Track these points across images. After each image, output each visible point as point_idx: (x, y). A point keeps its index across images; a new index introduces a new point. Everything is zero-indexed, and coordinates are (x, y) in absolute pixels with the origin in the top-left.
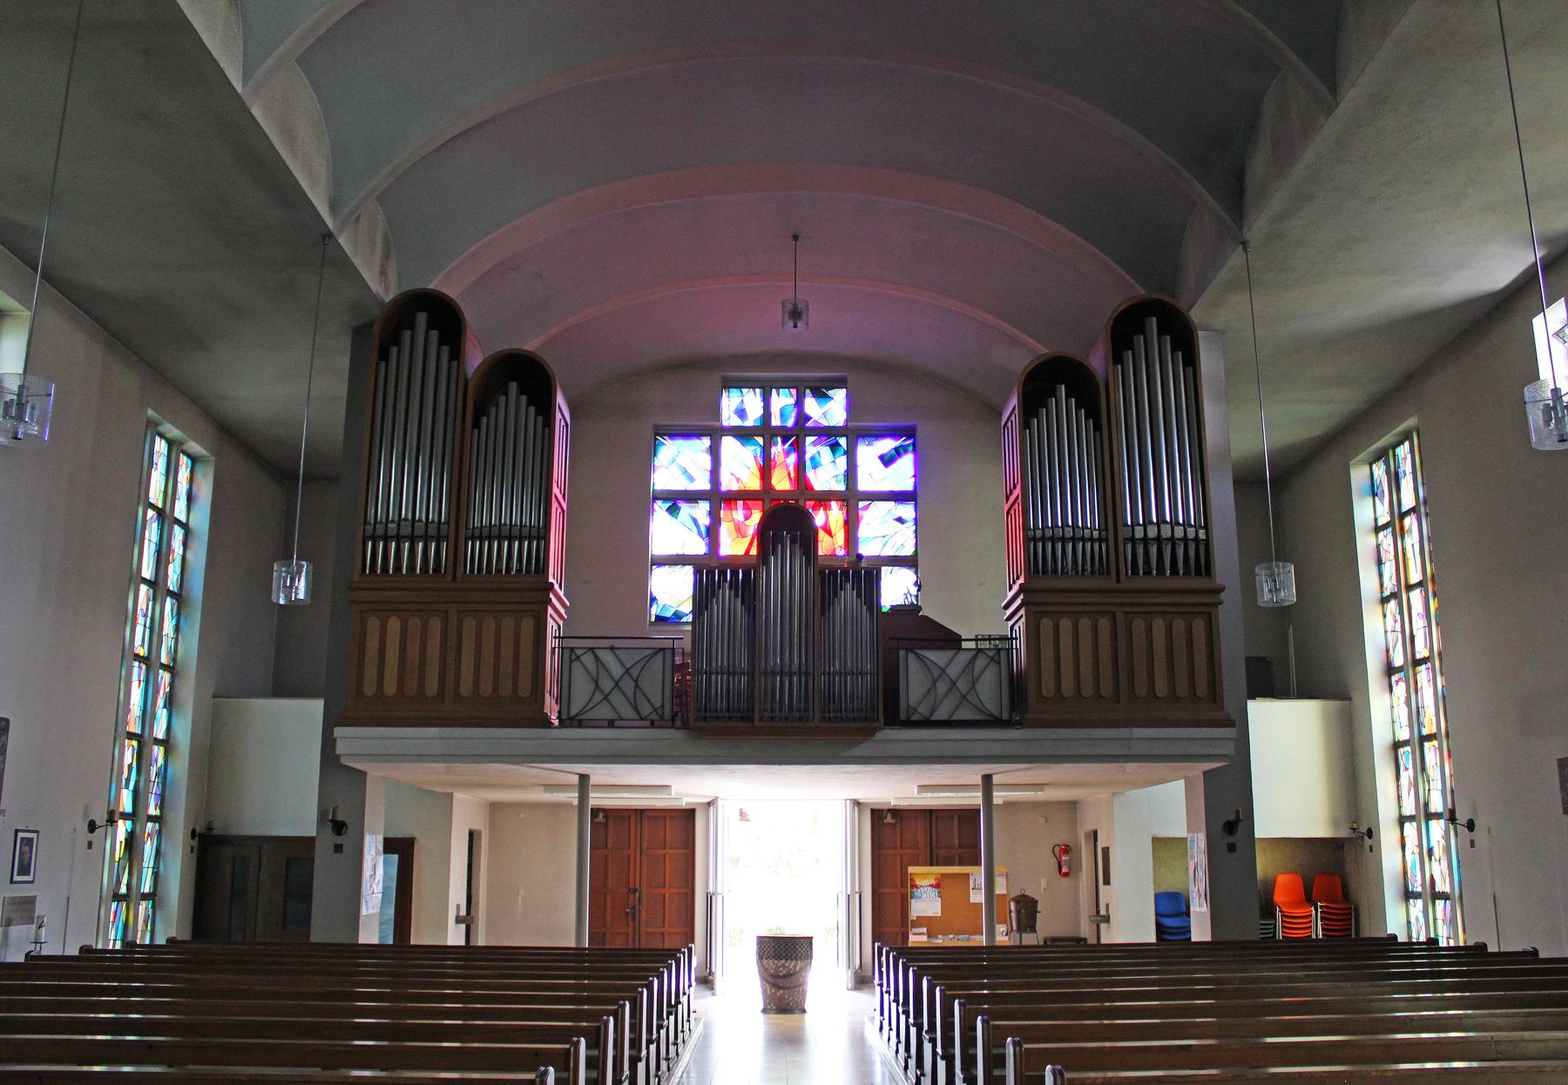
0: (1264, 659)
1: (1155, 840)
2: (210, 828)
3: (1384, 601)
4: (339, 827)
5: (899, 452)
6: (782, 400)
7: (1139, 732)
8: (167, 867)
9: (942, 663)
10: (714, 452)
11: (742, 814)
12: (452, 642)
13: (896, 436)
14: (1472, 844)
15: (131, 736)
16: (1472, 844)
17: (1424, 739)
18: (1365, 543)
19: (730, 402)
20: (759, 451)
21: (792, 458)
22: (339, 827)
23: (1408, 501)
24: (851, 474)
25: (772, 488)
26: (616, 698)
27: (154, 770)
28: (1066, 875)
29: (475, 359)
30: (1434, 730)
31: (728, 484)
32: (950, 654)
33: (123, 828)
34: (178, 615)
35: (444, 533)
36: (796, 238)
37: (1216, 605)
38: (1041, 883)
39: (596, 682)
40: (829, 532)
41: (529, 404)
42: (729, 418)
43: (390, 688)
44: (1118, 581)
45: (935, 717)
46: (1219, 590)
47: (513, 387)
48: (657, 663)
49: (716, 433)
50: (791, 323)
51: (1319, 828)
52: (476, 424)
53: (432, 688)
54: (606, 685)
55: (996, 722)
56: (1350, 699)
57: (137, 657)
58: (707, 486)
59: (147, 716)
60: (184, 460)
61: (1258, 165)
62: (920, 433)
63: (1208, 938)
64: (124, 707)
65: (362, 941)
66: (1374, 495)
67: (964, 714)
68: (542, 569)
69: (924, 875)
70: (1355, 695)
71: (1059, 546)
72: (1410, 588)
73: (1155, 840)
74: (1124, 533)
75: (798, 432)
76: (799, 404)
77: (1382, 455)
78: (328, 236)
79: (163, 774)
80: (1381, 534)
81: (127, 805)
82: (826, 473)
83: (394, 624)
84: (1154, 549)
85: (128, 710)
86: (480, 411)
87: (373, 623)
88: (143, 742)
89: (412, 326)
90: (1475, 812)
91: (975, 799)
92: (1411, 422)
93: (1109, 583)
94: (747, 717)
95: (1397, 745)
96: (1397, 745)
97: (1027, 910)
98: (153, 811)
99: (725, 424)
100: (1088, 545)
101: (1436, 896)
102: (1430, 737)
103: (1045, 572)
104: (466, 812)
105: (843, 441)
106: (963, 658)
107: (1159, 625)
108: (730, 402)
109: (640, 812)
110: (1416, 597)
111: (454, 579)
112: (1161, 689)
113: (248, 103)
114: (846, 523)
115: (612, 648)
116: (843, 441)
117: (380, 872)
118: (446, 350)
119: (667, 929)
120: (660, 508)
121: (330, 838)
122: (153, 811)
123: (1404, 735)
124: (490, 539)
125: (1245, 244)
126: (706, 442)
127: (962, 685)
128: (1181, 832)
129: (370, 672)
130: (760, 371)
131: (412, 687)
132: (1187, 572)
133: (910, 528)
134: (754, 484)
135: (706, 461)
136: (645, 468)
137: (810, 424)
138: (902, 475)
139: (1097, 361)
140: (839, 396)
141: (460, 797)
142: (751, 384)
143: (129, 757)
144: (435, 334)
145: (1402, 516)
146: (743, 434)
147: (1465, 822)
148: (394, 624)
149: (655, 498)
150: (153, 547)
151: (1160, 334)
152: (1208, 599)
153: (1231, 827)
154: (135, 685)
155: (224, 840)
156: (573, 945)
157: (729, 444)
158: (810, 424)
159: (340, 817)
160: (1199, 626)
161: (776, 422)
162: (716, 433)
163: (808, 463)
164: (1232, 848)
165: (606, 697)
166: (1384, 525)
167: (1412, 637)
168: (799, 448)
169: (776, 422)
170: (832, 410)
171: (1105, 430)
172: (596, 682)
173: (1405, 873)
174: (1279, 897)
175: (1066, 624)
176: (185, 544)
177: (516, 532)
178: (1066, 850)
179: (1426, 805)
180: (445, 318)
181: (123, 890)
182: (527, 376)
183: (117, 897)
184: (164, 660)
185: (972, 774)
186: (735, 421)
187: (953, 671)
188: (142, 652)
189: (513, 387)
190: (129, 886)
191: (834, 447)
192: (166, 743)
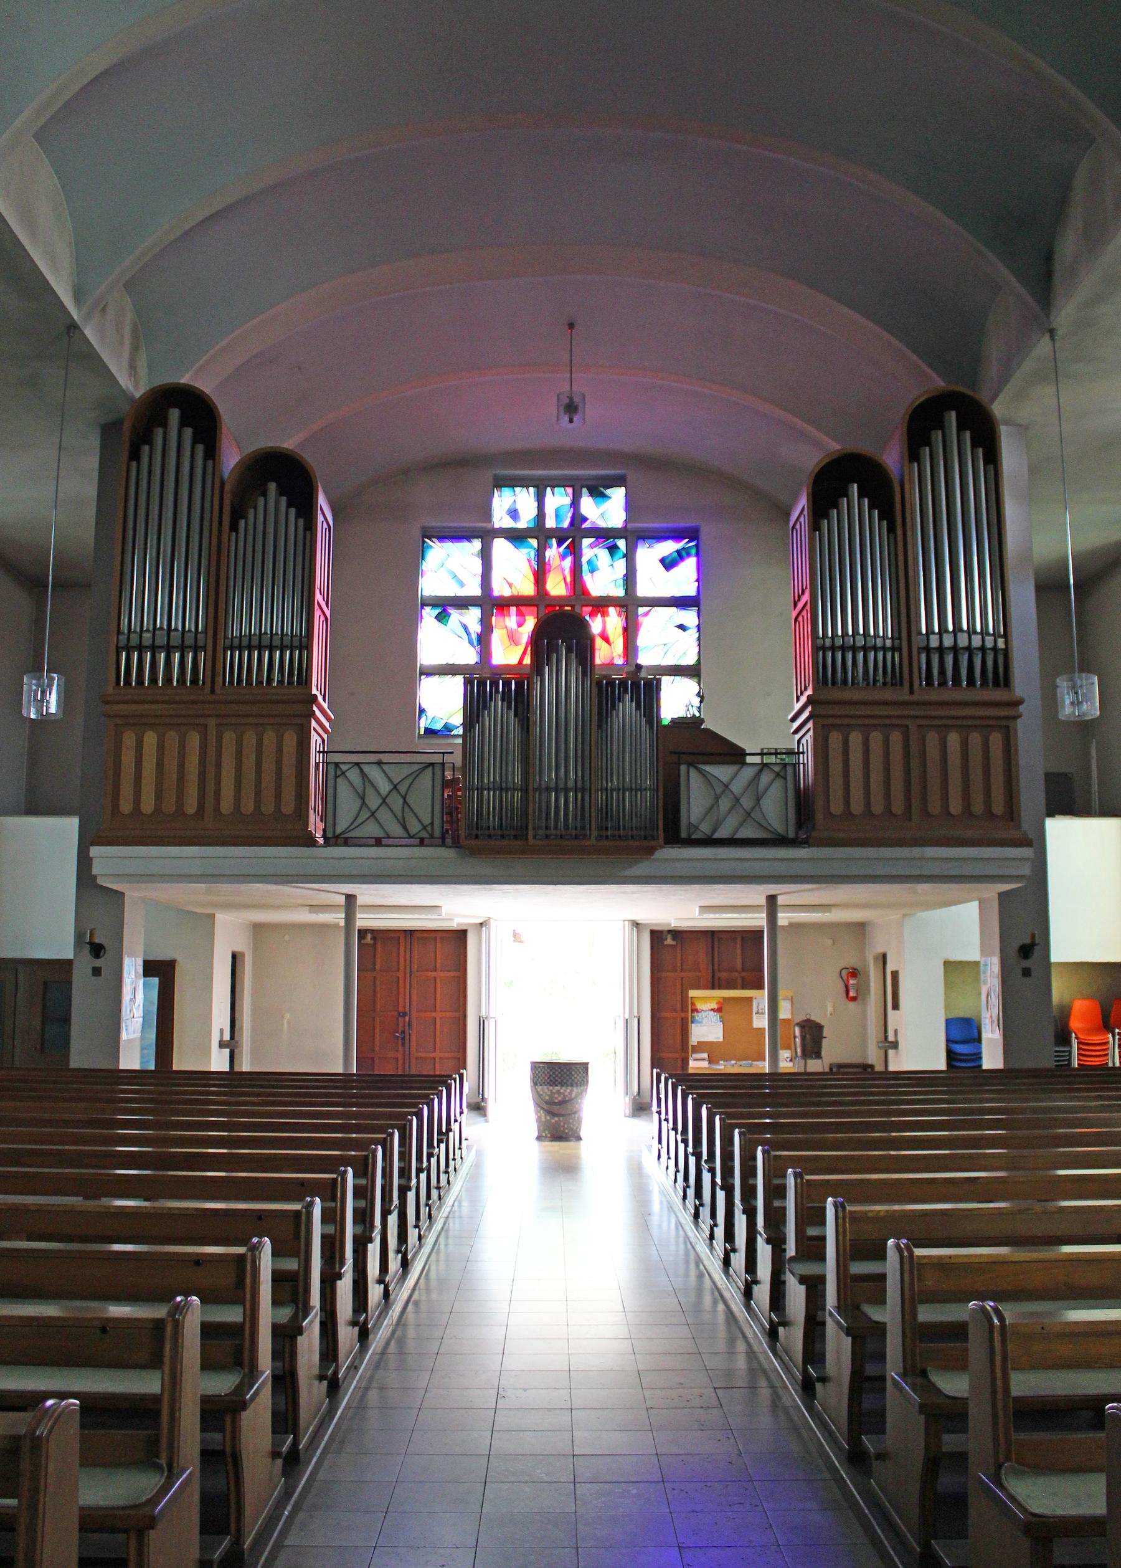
0: (1064, 775)
1: (947, 964)
4: (97, 950)
5: (681, 556)
6: (558, 500)
10: (486, 556)
13: (677, 538)
20: (533, 554)
21: (568, 562)
22: (97, 950)
24: (630, 579)
25: (547, 593)
26: (384, 815)
28: (854, 999)
29: (231, 459)
31: (500, 589)
35: (201, 643)
36: (571, 326)
38: (827, 1009)
39: (363, 798)
40: (606, 639)
42: (500, 519)
43: (148, 805)
44: (912, 692)
45: (717, 835)
47: (272, 487)
49: (487, 535)
50: (567, 418)
52: (234, 528)
53: (191, 807)
54: (373, 802)
55: (781, 841)
61: (1068, 247)
63: (1000, 1065)
68: (304, 680)
69: (705, 999)
73: (947, 964)
75: (574, 534)
76: (575, 504)
82: (604, 577)
83: (151, 739)
84: (949, 660)
86: (238, 514)
91: (759, 920)
93: (903, 695)
94: (520, 834)
97: (812, 1036)
100: (880, 655)
104: (229, 933)
105: (621, 543)
106: (747, 773)
107: (953, 738)
109: (410, 934)
111: (213, 691)
112: (956, 808)
114: (625, 630)
116: (621, 543)
118: (200, 448)
120: (429, 614)
125: (1052, 332)
126: (477, 544)
127: (746, 802)
130: (534, 468)
132: (984, 683)
134: (527, 588)
135: (477, 565)
136: (413, 573)
137: (586, 525)
138: (684, 579)
139: (892, 458)
140: (618, 495)
142: (524, 483)
146: (516, 537)
149: (423, 605)
153: (1026, 951)
157: (501, 547)
158: (586, 525)
159: (97, 940)
160: (996, 738)
161: (550, 523)
162: (487, 535)
163: (585, 567)
164: (1027, 972)
165: (373, 814)
168: (575, 551)
169: (550, 523)
170: (610, 510)
171: (899, 531)
174: (1075, 1023)
175: (855, 738)
178: (854, 973)
180: (198, 414)
182: (285, 476)
185: (757, 894)
186: (507, 523)
189: (272, 487)
191: (612, 549)
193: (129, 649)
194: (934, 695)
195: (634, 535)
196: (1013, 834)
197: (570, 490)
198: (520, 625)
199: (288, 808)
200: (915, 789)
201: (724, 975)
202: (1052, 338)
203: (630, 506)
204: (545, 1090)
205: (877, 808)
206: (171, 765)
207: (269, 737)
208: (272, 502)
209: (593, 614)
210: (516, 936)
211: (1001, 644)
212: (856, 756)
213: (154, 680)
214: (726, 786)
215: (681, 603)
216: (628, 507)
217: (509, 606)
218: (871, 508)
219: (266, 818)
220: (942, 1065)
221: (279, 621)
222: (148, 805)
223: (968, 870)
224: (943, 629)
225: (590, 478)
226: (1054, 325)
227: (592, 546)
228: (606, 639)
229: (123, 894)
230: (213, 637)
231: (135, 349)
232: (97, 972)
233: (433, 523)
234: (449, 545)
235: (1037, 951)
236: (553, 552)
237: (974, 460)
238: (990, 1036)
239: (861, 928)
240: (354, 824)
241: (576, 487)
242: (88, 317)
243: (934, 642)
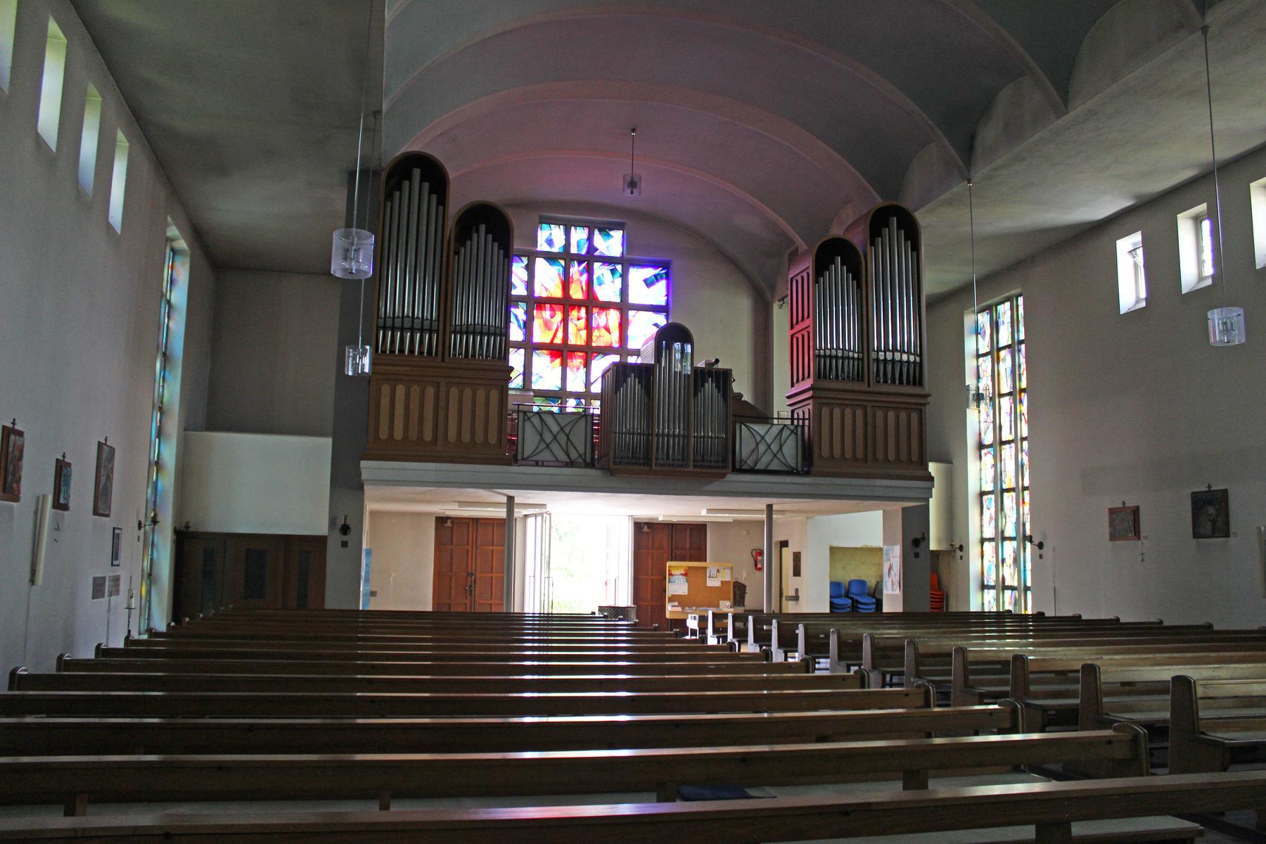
1: (832, 549)
2: (187, 527)
4: (345, 529)
5: (657, 278)
6: (579, 234)
7: (879, 482)
9: (762, 433)
12: (442, 403)
13: (656, 267)
14: (1041, 556)
16: (1041, 556)
19: (543, 234)
21: (585, 277)
23: (1005, 338)
24: (624, 291)
26: (555, 447)
29: (457, 202)
30: (1013, 485)
31: (539, 292)
35: (435, 327)
37: (924, 405)
39: (541, 435)
40: (608, 330)
41: (494, 241)
42: (542, 246)
43: (398, 435)
44: (443, 360)
45: (758, 467)
47: (483, 227)
48: (582, 423)
52: (457, 253)
53: (428, 436)
54: (548, 437)
55: (790, 472)
56: (951, 463)
58: (524, 293)
61: (989, 133)
62: (675, 267)
63: (900, 609)
66: (977, 333)
67: (775, 466)
69: (676, 568)
70: (957, 462)
72: (1001, 396)
73: (832, 549)
74: (873, 355)
75: (590, 258)
76: (590, 239)
80: (981, 359)
82: (608, 289)
83: (401, 390)
84: (889, 367)
89: (410, 178)
90: (1045, 538)
91: (501, 513)
93: (864, 387)
95: (982, 494)
96: (982, 494)
99: (539, 249)
101: (1005, 588)
102: (1008, 490)
105: (619, 267)
106: (775, 430)
107: (891, 415)
108: (543, 234)
109: (476, 521)
111: (443, 360)
112: (891, 457)
118: (434, 197)
123: (989, 487)
127: (775, 448)
128: (876, 540)
130: (566, 213)
131: (413, 434)
132: (908, 383)
134: (557, 293)
137: (597, 253)
139: (858, 238)
140: (617, 235)
142: (557, 222)
144: (426, 185)
145: (999, 349)
146: (551, 258)
147: (1036, 542)
148: (401, 390)
152: (923, 401)
153: (916, 542)
157: (540, 263)
158: (597, 253)
160: (914, 416)
161: (574, 250)
163: (595, 281)
165: (548, 446)
166: (991, 352)
168: (589, 270)
169: (574, 250)
170: (612, 244)
172: (541, 435)
175: (837, 411)
177: (417, 324)
179: (1003, 532)
180: (432, 173)
185: (761, 503)
187: (769, 439)
189: (483, 227)
191: (613, 271)
193: (385, 329)
194: (885, 388)
195: (624, 263)
196: (918, 473)
197: (586, 230)
198: (552, 317)
200: (870, 441)
201: (679, 552)
203: (626, 242)
205: (848, 455)
206: (414, 406)
207: (481, 394)
208: (481, 235)
212: (837, 422)
220: (827, 610)
224: (886, 349)
228: (608, 330)
230: (443, 324)
235: (922, 544)
236: (575, 270)
237: (905, 247)
238: (890, 592)
240: (534, 454)
241: (591, 227)
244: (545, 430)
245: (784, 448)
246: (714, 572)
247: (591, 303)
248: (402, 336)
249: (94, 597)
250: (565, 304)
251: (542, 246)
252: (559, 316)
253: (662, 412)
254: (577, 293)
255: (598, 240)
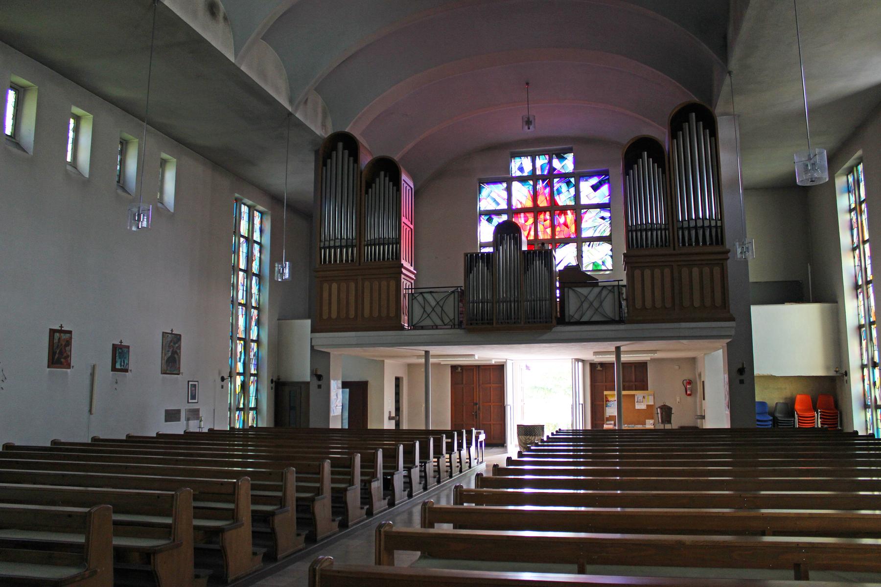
0: (797, 282)
3: (854, 249)
4: (319, 377)
6: (541, 161)
7: (683, 325)
8: (259, 396)
10: (509, 190)
11: (527, 367)
15: (240, 339)
17: (871, 323)
18: (843, 218)
19: (515, 164)
20: (531, 188)
21: (547, 190)
22: (319, 377)
25: (538, 206)
26: (433, 315)
27: (252, 354)
28: (690, 395)
29: (365, 160)
31: (516, 204)
32: (589, 289)
33: (239, 380)
34: (260, 284)
36: (527, 84)
37: (727, 259)
38: (675, 399)
42: (516, 173)
43: (334, 315)
44: (674, 249)
46: (728, 252)
47: (382, 173)
49: (509, 180)
50: (527, 127)
51: (819, 372)
52: (367, 192)
53: (352, 314)
54: (429, 310)
56: (837, 302)
57: (240, 304)
58: (506, 207)
59: (247, 330)
60: (256, 214)
63: (726, 425)
64: (234, 327)
65: (331, 427)
66: (849, 192)
67: (596, 318)
68: (398, 257)
71: (644, 233)
75: (551, 175)
76: (550, 162)
77: (850, 171)
78: (290, 114)
79: (257, 355)
81: (240, 368)
82: (565, 198)
83: (335, 286)
84: (701, 232)
85: (238, 328)
86: (369, 185)
87: (326, 286)
88: (246, 341)
91: (612, 358)
92: (859, 153)
93: (671, 251)
94: (490, 322)
95: (860, 327)
97: (667, 412)
98: (253, 371)
100: (659, 232)
103: (647, 246)
104: (392, 369)
105: (572, 180)
107: (696, 271)
110: (867, 246)
112: (697, 304)
113: (238, 65)
114: (575, 221)
115: (431, 292)
116: (572, 180)
117: (340, 396)
118: (351, 159)
119: (492, 422)
120: (484, 219)
121: (315, 382)
122: (253, 371)
123: (863, 322)
124: (375, 245)
125: (730, 73)
126: (505, 185)
127: (596, 304)
129: (325, 308)
130: (530, 148)
133: (607, 223)
134: (529, 204)
135: (505, 194)
136: (474, 199)
138: (603, 195)
140: (570, 157)
141: (388, 362)
142: (525, 155)
143: (240, 348)
145: (861, 203)
146: (522, 180)
148: (335, 286)
149: (480, 215)
150: (245, 255)
151: (697, 122)
152: (723, 256)
153: (741, 371)
154: (240, 316)
155: (284, 384)
156: (424, 428)
157: (516, 185)
159: (319, 373)
160: (717, 270)
161: (538, 172)
162: (509, 180)
163: (555, 192)
164: (742, 382)
167: (866, 269)
168: (550, 185)
169: (538, 172)
170: (567, 164)
171: (667, 172)
173: (864, 395)
174: (797, 407)
175: (648, 273)
176: (260, 252)
178: (690, 382)
180: (350, 143)
181: (241, 406)
182: (387, 169)
183: (238, 409)
184: (254, 305)
185: (611, 346)
186: (519, 174)
187: (591, 297)
188: (243, 302)
190: (244, 404)
191: (568, 183)
192: (257, 341)
193: (325, 248)
195: (573, 178)
198: (526, 221)
199: (392, 314)
202: (730, 75)
204: (523, 437)
205: (658, 304)
206: (343, 295)
209: (560, 215)
210: (527, 367)
211: (719, 223)
213: (335, 261)
214: (586, 297)
215: (602, 206)
216: (574, 163)
217: (520, 213)
218: (653, 163)
219: (383, 320)
221: (387, 233)
222: (334, 315)
223: (704, 333)
225: (557, 150)
226: (730, 69)
227: (558, 182)
228: (567, 226)
229: (329, 353)
231: (324, 118)
232: (319, 387)
233: (483, 176)
234: (492, 186)
239: (693, 360)
241: (551, 154)
242: (296, 109)
243: (686, 225)
244: (427, 305)
245: (603, 304)
246: (641, 398)
247: (555, 209)
248: (652, 234)
249: (166, 421)
250: (536, 210)
251: (516, 173)
252: (531, 221)
253: (502, 286)
254: (542, 202)
255: (556, 163)
